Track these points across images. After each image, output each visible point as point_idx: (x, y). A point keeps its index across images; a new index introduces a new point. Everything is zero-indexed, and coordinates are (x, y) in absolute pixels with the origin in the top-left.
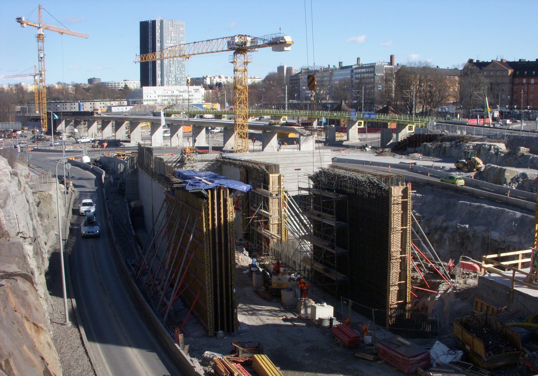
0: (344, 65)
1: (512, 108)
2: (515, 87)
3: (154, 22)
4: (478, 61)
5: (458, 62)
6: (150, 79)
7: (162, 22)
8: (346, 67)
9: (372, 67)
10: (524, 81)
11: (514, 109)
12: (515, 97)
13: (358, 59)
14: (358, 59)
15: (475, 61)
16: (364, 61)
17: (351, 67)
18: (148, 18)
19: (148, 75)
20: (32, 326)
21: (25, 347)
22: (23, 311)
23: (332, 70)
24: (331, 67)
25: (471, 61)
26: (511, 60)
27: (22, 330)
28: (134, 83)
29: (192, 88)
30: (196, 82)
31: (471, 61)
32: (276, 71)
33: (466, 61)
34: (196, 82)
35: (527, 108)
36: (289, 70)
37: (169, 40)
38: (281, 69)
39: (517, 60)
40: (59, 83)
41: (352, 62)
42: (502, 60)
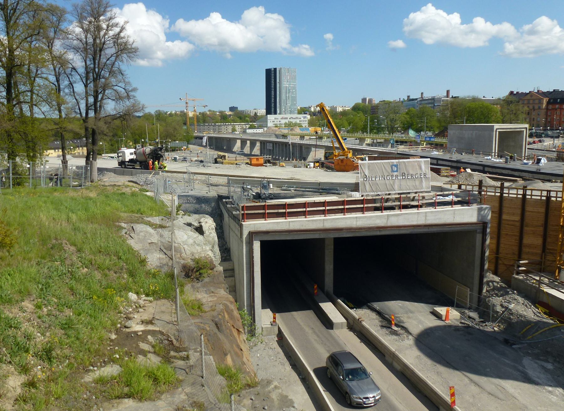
0: (411, 98)
1: (545, 130)
2: (549, 113)
3: (275, 69)
4: (517, 93)
5: (503, 94)
6: (273, 109)
7: (280, 69)
8: (413, 100)
9: (433, 100)
10: (557, 106)
11: (548, 130)
12: (549, 120)
13: (422, 93)
14: (422, 93)
15: (515, 93)
16: (427, 96)
17: (416, 99)
18: (272, 67)
19: (271, 108)
20: (236, 331)
21: (234, 346)
22: (231, 322)
23: (402, 102)
24: (402, 100)
25: (512, 93)
26: (545, 90)
27: (232, 335)
28: (262, 111)
29: (301, 116)
30: (303, 111)
31: (512, 93)
32: (360, 102)
33: (507, 93)
34: (303, 111)
35: (559, 129)
36: (370, 101)
37: (284, 83)
38: (364, 100)
39: (551, 90)
40: (209, 111)
41: (418, 96)
42: (538, 91)
